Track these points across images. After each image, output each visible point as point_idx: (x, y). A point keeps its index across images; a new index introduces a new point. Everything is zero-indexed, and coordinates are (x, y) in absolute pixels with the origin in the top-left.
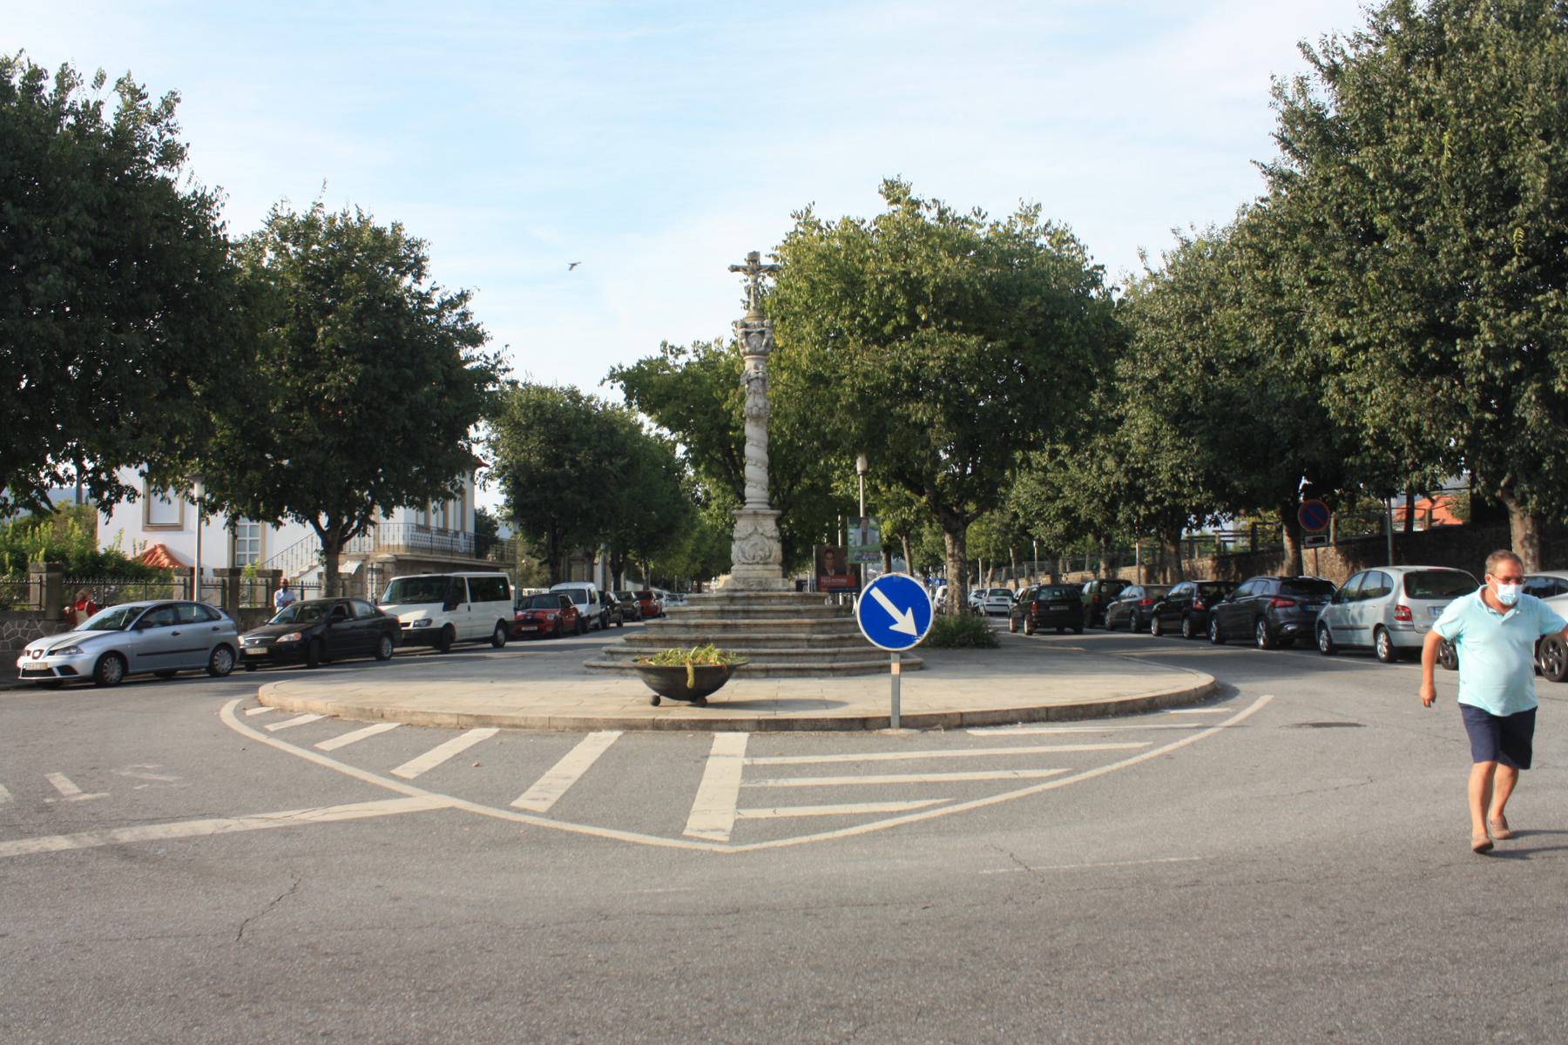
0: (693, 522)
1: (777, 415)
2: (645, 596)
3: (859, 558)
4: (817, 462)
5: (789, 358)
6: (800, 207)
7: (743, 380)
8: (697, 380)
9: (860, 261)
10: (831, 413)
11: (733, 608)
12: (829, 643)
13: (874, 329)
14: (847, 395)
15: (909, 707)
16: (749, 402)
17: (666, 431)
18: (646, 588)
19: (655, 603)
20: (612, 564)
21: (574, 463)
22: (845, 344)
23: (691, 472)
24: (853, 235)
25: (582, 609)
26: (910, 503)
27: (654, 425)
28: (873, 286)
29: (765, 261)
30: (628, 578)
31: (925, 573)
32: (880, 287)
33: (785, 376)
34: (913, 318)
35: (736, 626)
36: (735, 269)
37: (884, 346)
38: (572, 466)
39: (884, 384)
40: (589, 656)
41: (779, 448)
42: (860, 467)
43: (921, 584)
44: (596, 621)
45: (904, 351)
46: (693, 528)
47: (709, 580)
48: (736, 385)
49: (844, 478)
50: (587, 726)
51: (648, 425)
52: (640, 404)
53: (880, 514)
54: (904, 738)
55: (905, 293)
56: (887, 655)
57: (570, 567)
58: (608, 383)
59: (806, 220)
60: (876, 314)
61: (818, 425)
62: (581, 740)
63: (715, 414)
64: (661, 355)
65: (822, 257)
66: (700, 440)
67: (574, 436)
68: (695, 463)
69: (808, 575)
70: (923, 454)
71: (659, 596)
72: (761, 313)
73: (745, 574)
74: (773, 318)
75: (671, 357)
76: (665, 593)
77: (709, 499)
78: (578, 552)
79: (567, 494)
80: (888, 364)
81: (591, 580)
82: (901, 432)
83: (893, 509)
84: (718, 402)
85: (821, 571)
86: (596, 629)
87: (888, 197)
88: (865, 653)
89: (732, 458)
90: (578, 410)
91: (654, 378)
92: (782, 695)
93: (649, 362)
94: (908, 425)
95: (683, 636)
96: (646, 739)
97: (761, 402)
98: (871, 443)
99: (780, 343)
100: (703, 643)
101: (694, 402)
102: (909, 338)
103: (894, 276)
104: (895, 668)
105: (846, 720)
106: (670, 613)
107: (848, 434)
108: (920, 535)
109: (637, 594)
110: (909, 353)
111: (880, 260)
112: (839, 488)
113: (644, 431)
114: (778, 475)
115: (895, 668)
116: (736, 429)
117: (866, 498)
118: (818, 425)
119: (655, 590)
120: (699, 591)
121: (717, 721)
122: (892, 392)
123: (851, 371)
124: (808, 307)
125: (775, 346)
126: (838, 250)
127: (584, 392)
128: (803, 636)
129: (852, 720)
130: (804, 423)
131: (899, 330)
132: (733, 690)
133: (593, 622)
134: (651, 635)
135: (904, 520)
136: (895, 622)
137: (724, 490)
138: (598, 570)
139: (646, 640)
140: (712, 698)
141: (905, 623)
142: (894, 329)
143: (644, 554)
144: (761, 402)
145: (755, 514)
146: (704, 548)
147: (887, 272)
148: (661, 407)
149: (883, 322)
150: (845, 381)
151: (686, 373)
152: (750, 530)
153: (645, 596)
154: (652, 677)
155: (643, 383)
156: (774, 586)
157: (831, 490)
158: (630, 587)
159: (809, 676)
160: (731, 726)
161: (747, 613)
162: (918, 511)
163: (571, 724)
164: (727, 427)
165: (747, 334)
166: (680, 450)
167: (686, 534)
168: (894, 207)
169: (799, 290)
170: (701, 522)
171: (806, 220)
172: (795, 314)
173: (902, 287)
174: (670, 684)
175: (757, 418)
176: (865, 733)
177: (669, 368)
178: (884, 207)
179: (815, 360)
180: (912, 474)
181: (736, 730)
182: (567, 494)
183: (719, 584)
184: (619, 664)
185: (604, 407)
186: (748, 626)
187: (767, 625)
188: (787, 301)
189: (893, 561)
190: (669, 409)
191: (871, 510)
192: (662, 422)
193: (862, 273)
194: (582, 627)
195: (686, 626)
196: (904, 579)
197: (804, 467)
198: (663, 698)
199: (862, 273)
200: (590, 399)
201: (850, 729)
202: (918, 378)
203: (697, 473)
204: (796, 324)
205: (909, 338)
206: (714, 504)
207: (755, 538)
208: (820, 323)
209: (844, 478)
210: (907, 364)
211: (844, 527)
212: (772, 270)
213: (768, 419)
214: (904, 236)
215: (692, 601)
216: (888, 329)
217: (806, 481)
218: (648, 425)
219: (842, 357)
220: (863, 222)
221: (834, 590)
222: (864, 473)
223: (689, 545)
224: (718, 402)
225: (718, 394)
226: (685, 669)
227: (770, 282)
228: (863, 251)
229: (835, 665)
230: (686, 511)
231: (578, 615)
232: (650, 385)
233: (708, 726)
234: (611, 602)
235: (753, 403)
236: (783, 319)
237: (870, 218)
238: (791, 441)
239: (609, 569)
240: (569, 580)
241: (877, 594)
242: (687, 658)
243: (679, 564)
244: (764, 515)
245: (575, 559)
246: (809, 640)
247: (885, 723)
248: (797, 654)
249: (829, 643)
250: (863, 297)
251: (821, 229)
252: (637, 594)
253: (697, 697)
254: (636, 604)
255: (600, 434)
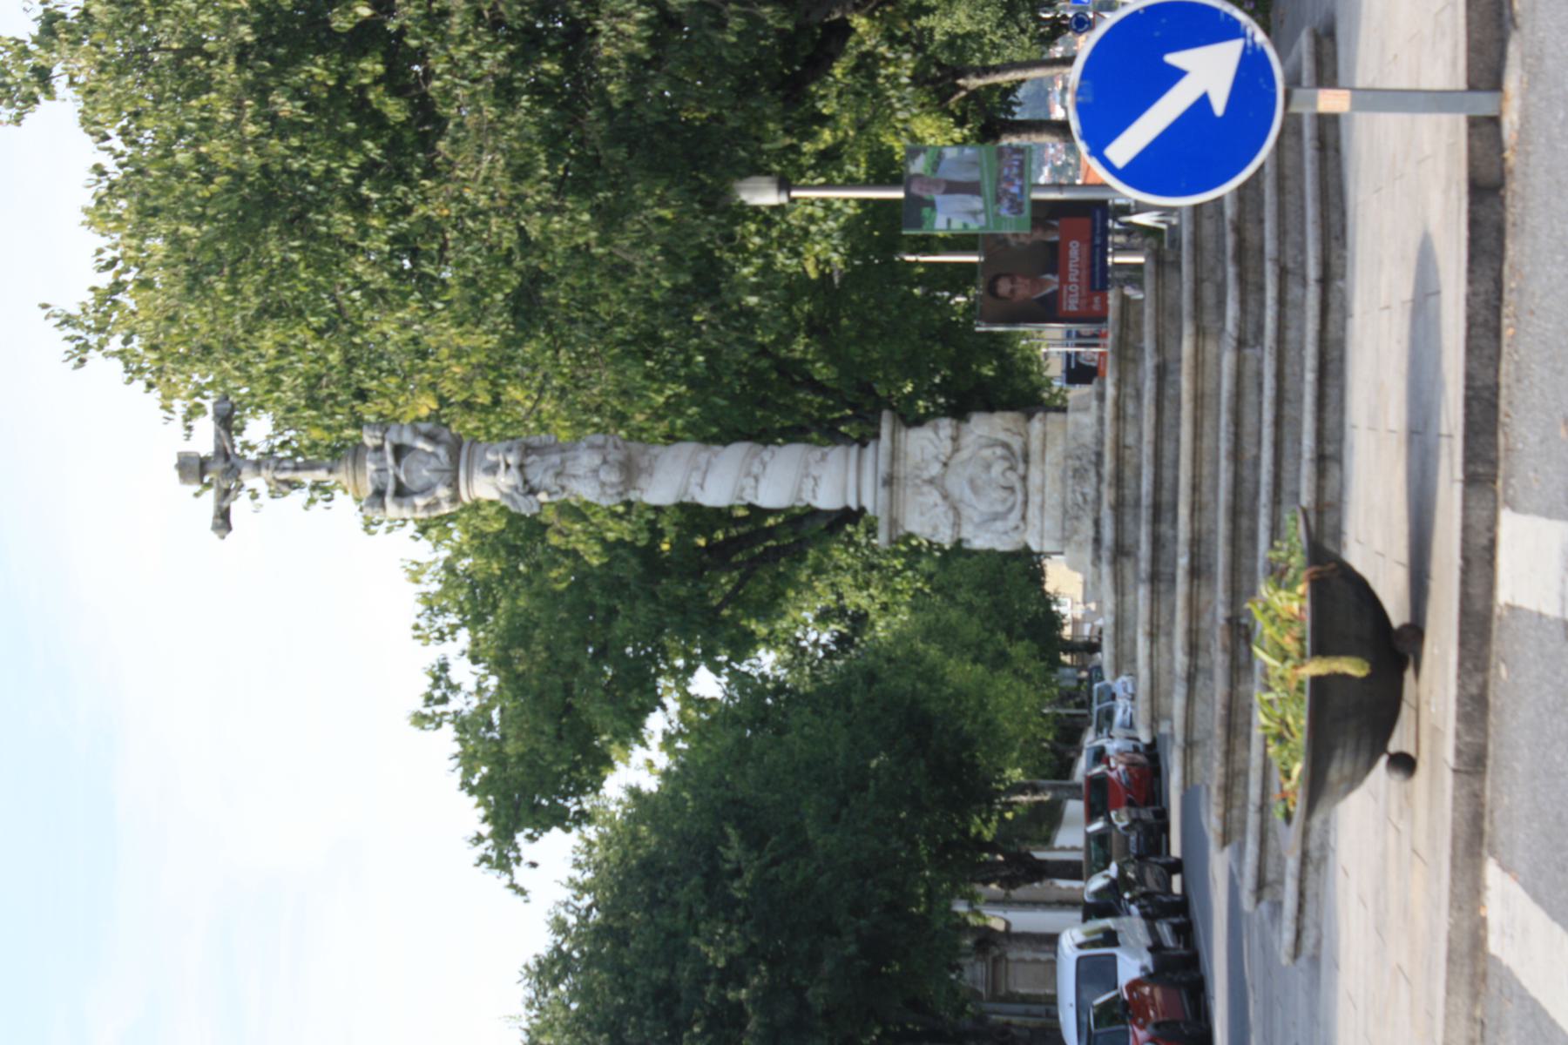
0: (901, 658)
1: (621, 418)
2: (1099, 796)
3: (1016, 206)
4: (749, 313)
5: (467, 381)
6: (57, 342)
7: (526, 507)
8: (518, 634)
9: (207, 179)
10: (619, 272)
11: (1145, 549)
12: (1250, 288)
13: (394, 147)
14: (575, 224)
15: (1442, 63)
16: (584, 490)
17: (656, 723)
18: (1075, 792)
19: (1117, 769)
20: (1010, 883)
21: (734, 974)
22: (432, 227)
23: (766, 661)
24: (136, 198)
25: (1130, 966)
26: (867, 64)
27: (638, 754)
28: (276, 146)
29: (204, 440)
30: (1047, 841)
31: (1057, 29)
32: (279, 127)
33: (514, 393)
34: (366, 37)
35: (1196, 542)
36: (223, 521)
37: (441, 122)
38: (742, 983)
39: (543, 125)
40: (1267, 948)
41: (712, 415)
42: (763, 195)
43: (1085, 45)
44: (1164, 929)
45: (455, 66)
46: (915, 658)
47: (1055, 621)
48: (535, 528)
49: (795, 240)
50: (1471, 959)
51: (638, 771)
52: (580, 790)
53: (899, 146)
54: (1533, 77)
55: (295, 59)
56: (1293, 125)
57: (1012, 998)
58: (522, 874)
59: (90, 328)
60: (353, 142)
61: (652, 306)
62: (1508, 976)
63: (614, 586)
64: (448, 731)
65: (195, 283)
66: (685, 631)
67: (661, 974)
68: (743, 645)
69: (1050, 346)
70: (736, 24)
71: (1100, 756)
72: (343, 453)
73: (1053, 513)
74: (358, 423)
75: (457, 703)
76: (1090, 739)
77: (842, 612)
78: (974, 973)
79: (817, 996)
80: (490, 112)
81: (1052, 940)
82: (676, 82)
83: (882, 110)
84: (584, 577)
85: (1047, 311)
86: (1185, 931)
87: (31, 100)
88: (1280, 189)
89: (731, 544)
90: (590, 960)
91: (511, 748)
92: (1396, 416)
93: (468, 761)
94: (656, 62)
95: (1220, 688)
96: (1512, 796)
97: (586, 460)
98: (701, 160)
99: (426, 405)
100: (1240, 632)
101: (582, 642)
102: (421, 55)
103: (250, 87)
104: (1331, 101)
105: (1473, 242)
106: (1154, 721)
107: (677, 224)
108: (952, 41)
109: (1091, 816)
110: (462, 53)
111: (206, 124)
112: (824, 254)
113: (650, 784)
114: (779, 422)
115: (1331, 101)
116: (656, 534)
117: (852, 182)
118: (652, 306)
119: (1082, 769)
120: (1093, 647)
121: (1465, 597)
122: (567, 100)
123: (507, 212)
124: (331, 326)
125: (435, 417)
126: (177, 241)
127: (543, 942)
128: (1228, 360)
129: (1473, 224)
130: (644, 344)
131: (395, 82)
132: (1374, 550)
133: (1168, 939)
134: (1213, 773)
135: (916, 79)
136: (1204, 102)
137: (818, 570)
138: (1025, 920)
139: (1227, 790)
140: (1397, 612)
141: (1208, 73)
142: (397, 91)
143: (981, 794)
144: (586, 460)
145: (890, 481)
146: (972, 630)
147: (239, 106)
148: (592, 733)
149: (375, 121)
150: (534, 232)
151: (501, 664)
152: (934, 496)
153: (1099, 796)
154: (1334, 774)
155: (523, 784)
156: (1088, 436)
157: (825, 278)
158: (1071, 837)
159: (1341, 344)
160: (1480, 558)
161: (1161, 511)
162: (891, 39)
163: (1462, 1001)
164: (648, 554)
165: (401, 492)
166: (706, 684)
167: (932, 677)
168: (60, 84)
169: (283, 351)
170: (900, 638)
171: (90, 328)
172: (350, 363)
173: (282, 67)
174: (1357, 721)
175: (630, 471)
176: (1514, 186)
177: (485, 709)
178: (60, 112)
179: (474, 313)
180: (789, 56)
181: (1492, 546)
182: (817, 996)
183: (1069, 586)
184: (1292, 864)
185: (583, 889)
186: (1196, 509)
187: (1198, 461)
188: (314, 382)
189: (1021, 115)
190: (595, 710)
191: (885, 170)
192: (632, 731)
193: (239, 176)
194: (1180, 969)
195: (1191, 678)
196: (1085, 75)
197: (763, 351)
198: (1394, 746)
199: (239, 176)
200: (560, 927)
201: (1500, 231)
202: (529, 29)
203: (770, 641)
204: (376, 360)
205: (421, 55)
206: (855, 599)
207: (957, 484)
208: (375, 296)
209: (795, 240)
210: (492, 61)
211: (927, 244)
212: (227, 422)
213: (629, 434)
214: (138, 59)
215: (1124, 661)
216: (395, 110)
217: (800, 343)
218: (638, 771)
219: (467, 237)
220: (99, 170)
221: (1099, 277)
222: (784, 185)
223: (961, 672)
224: (584, 577)
225: (559, 577)
226: (1317, 681)
227: (258, 430)
228: (181, 174)
229: (1313, 272)
230: (871, 677)
231: (1150, 978)
232: (529, 760)
233: (1477, 623)
234: (1114, 887)
235: (588, 481)
236: (362, 395)
237: (87, 152)
238: (692, 381)
239: (1020, 893)
240: (1052, 1001)
241: (1124, 149)
242: (1284, 675)
243: (1015, 703)
244: (894, 457)
245: (994, 984)
246: (1241, 343)
247: (1485, 130)
248: (1279, 376)
249: (1250, 288)
250: (305, 175)
251: (118, 286)
252: (1091, 816)
253: (1395, 650)
254: (1121, 818)
255: (655, 902)
